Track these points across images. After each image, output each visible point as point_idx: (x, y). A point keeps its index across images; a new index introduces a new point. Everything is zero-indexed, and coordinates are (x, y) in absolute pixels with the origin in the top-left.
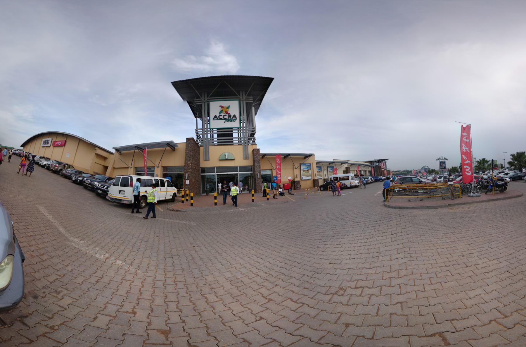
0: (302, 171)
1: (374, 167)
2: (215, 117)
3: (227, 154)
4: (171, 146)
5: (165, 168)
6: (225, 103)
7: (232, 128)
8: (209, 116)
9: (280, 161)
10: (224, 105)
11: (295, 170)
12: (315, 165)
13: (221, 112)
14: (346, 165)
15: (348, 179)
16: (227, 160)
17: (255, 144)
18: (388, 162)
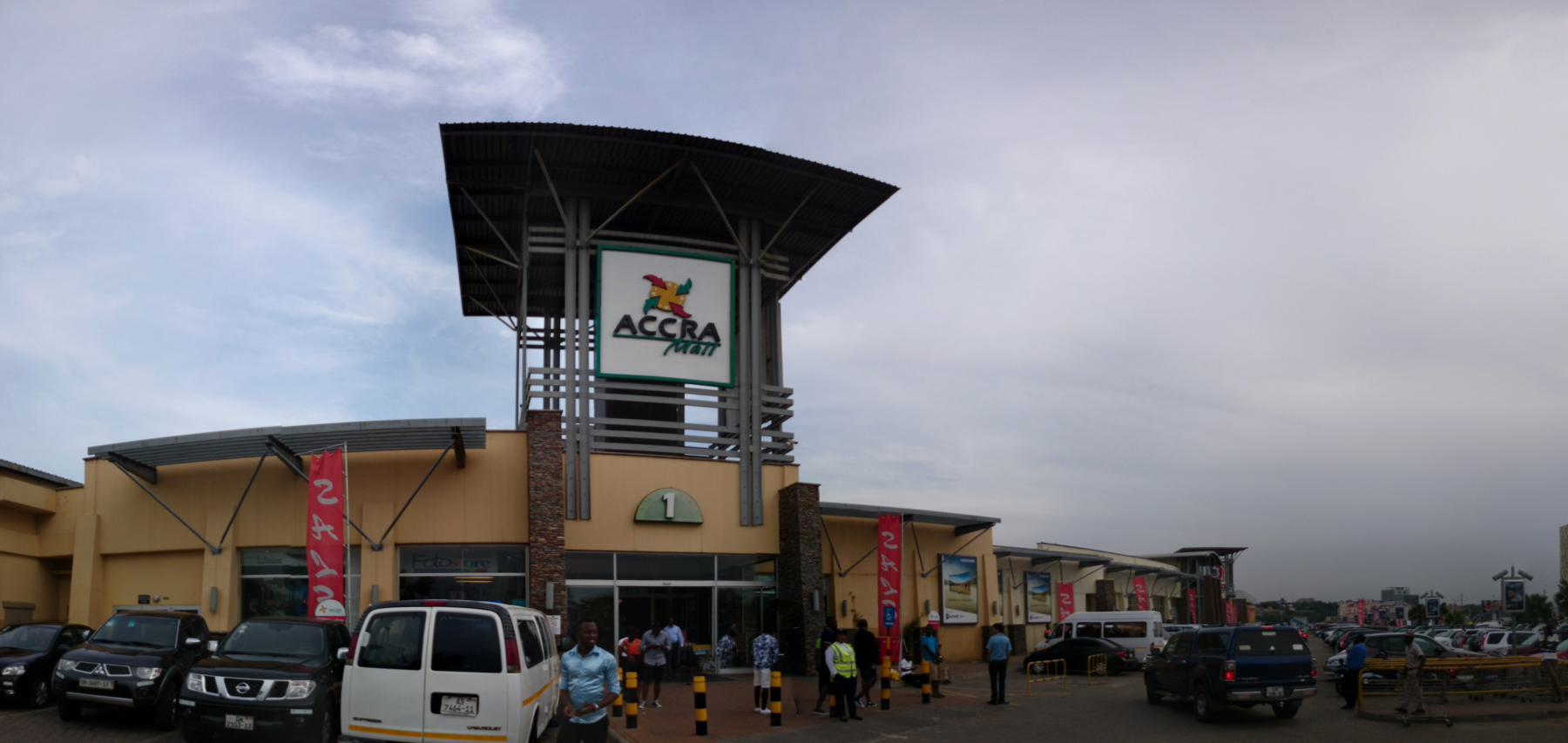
0: (946, 588)
1: (1194, 585)
2: (626, 322)
3: (670, 497)
4: (460, 440)
5: (410, 554)
6: (673, 269)
7: (680, 383)
8: (594, 313)
9: (897, 541)
10: (666, 277)
11: (920, 580)
12: (992, 566)
13: (652, 303)
14: (1099, 573)
15: (1143, 634)
16: (669, 522)
17: (789, 463)
18: (1239, 561)
